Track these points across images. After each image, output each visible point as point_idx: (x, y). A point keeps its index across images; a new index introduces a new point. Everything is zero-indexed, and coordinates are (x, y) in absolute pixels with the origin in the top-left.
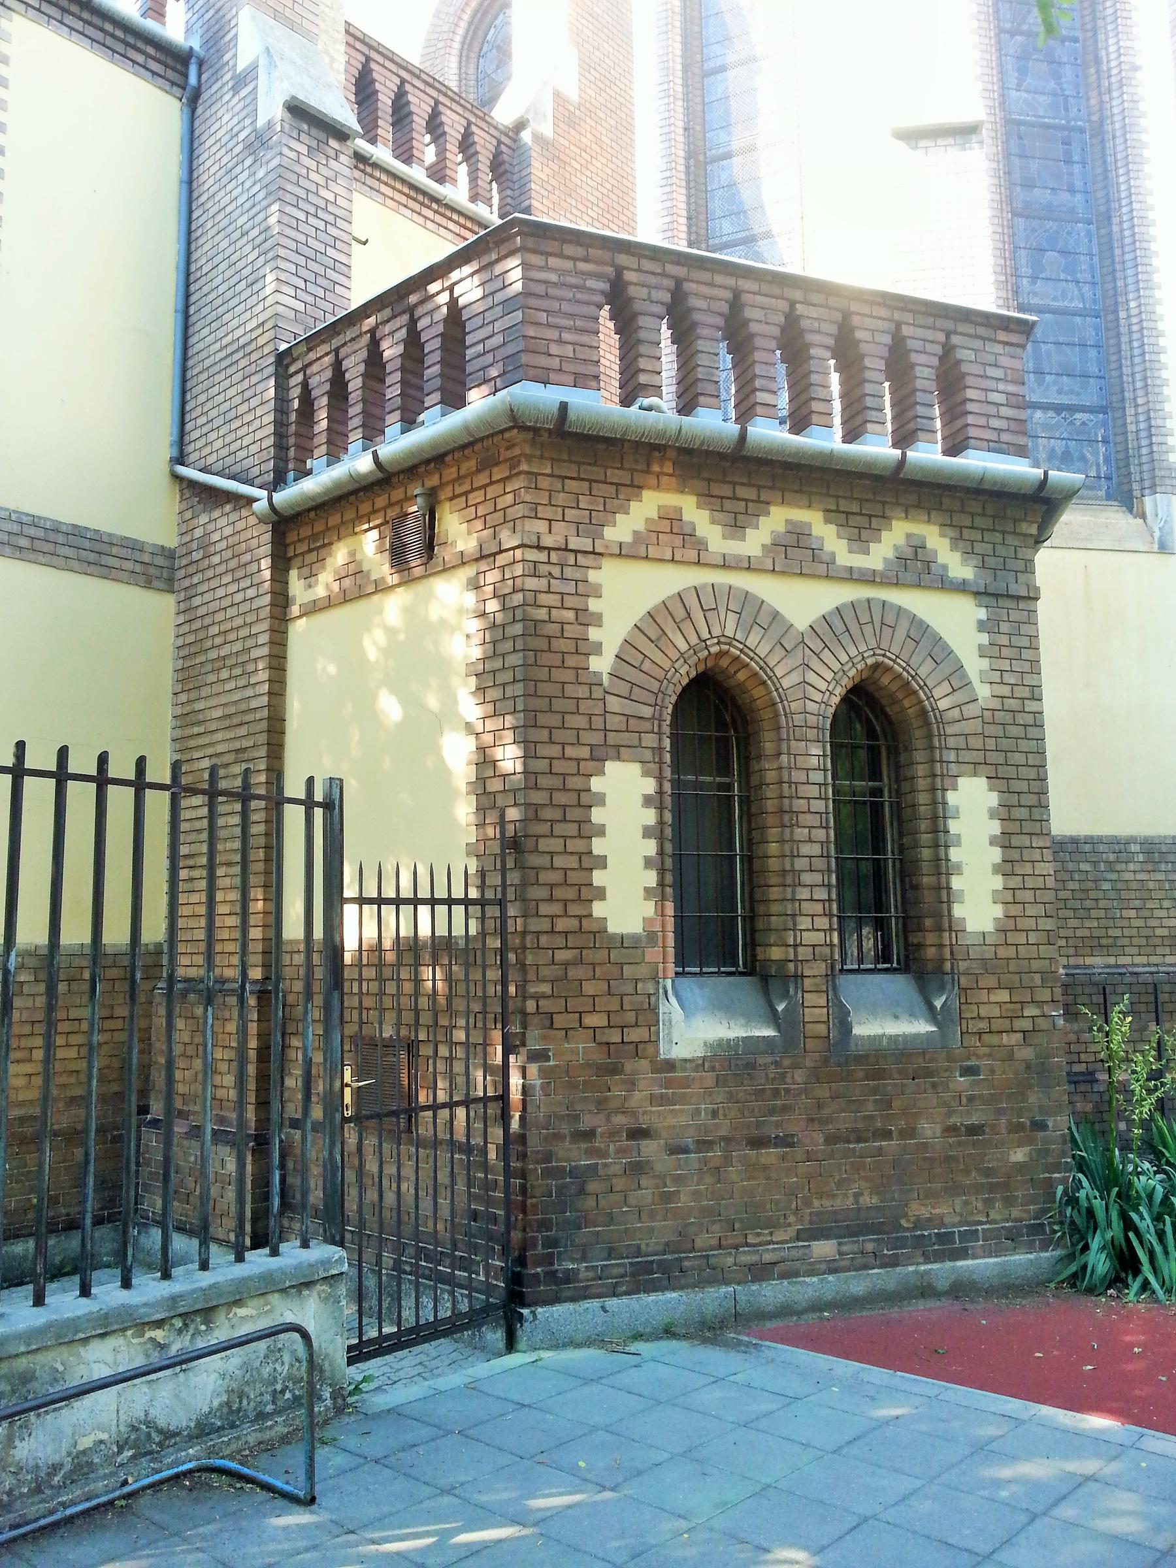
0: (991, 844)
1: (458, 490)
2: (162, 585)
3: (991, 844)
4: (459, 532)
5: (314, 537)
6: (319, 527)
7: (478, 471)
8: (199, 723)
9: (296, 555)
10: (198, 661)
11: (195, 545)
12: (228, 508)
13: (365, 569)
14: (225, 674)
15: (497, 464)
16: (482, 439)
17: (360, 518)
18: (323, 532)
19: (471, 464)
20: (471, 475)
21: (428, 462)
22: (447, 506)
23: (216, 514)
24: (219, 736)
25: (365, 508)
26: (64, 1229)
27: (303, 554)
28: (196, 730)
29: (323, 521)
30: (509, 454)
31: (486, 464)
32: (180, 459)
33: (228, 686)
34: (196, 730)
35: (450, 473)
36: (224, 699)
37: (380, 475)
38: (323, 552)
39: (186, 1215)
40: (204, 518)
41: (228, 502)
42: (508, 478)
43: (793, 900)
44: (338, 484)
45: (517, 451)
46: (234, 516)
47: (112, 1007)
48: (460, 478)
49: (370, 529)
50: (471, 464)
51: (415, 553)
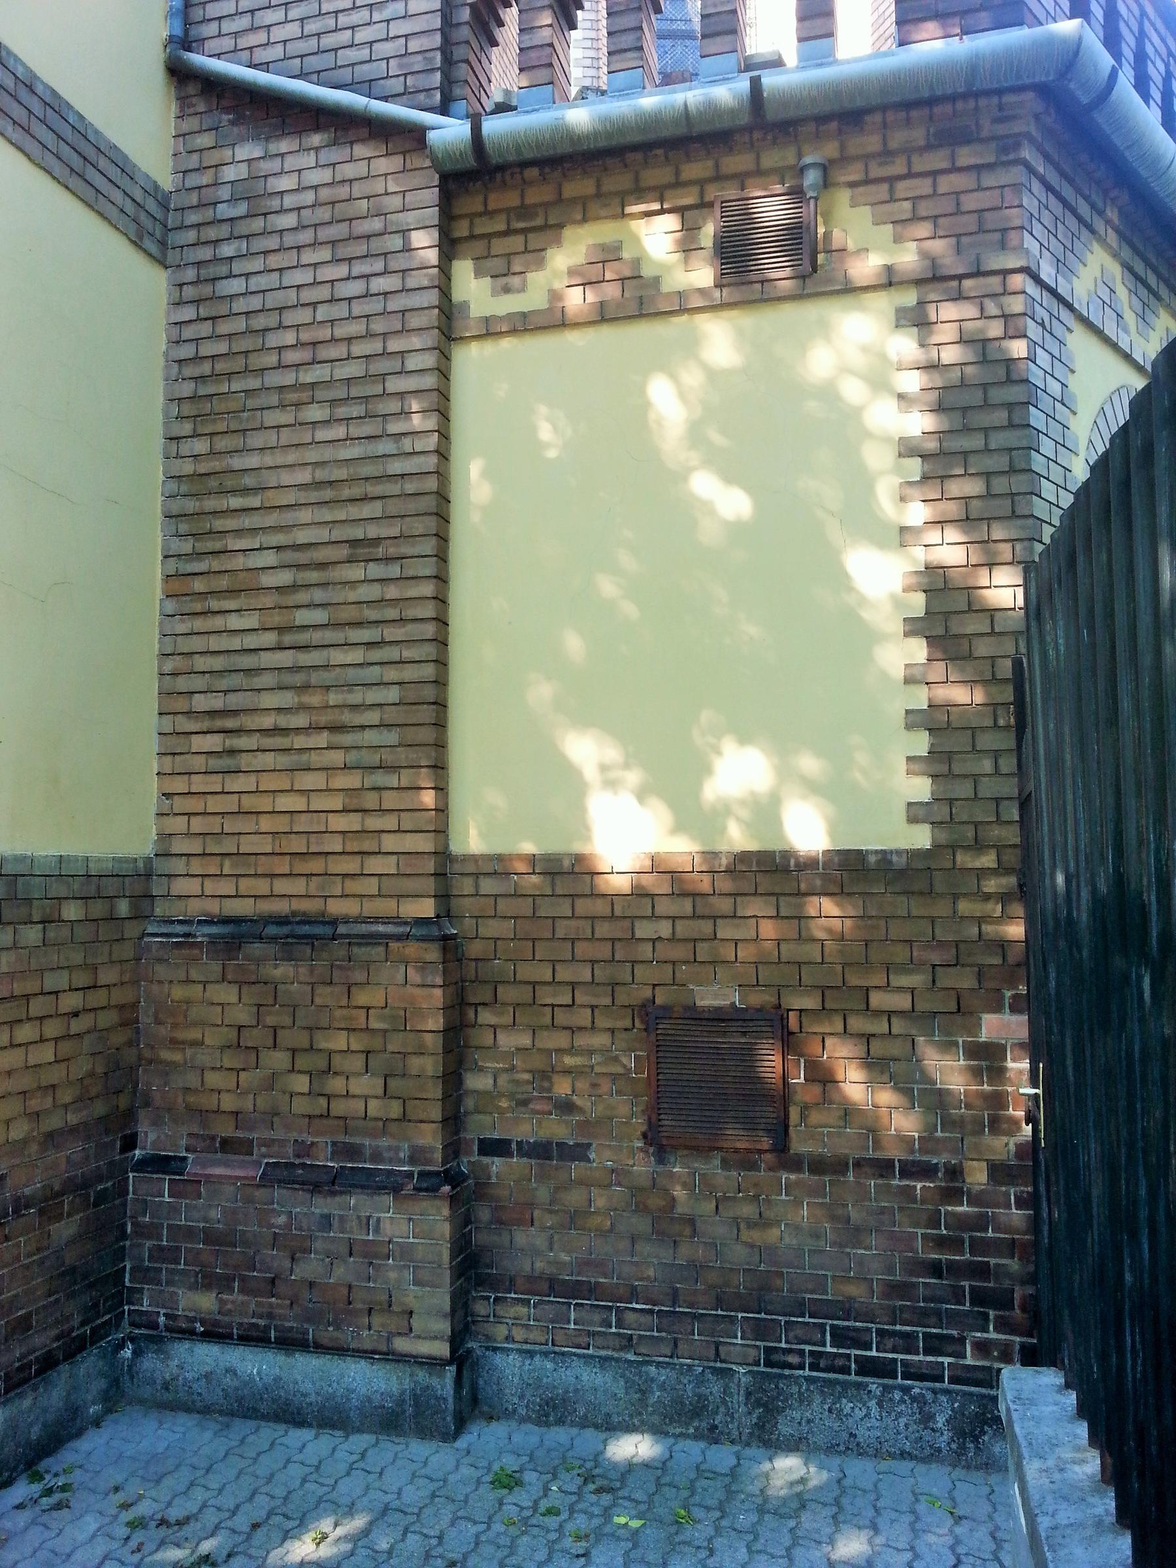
0: (909, 727)
1: (876, 171)
2: (153, 248)
3: (909, 727)
4: (869, 242)
5: (524, 211)
6: (534, 196)
7: (929, 147)
8: (246, 491)
9: (472, 237)
10: (235, 386)
11: (225, 193)
12: (316, 139)
13: (647, 272)
14: (315, 413)
15: (968, 142)
16: (953, 98)
17: (639, 193)
18: (546, 205)
19: (918, 135)
20: (908, 151)
21: (821, 119)
22: (843, 197)
23: (284, 146)
24: (305, 516)
25: (662, 175)
26: (39, 1373)
27: (488, 236)
28: (235, 502)
29: (480, 198)
30: (1001, 129)
31: (951, 137)
32: (185, 41)
33: (322, 434)
34: (235, 502)
35: (871, 142)
36: (312, 455)
37: (472, 162)
38: (535, 240)
39: (270, 1316)
40: (245, 151)
41: (317, 128)
42: (990, 167)
43: (951, 801)
44: (652, 121)
45: (1017, 127)
46: (334, 155)
47: (95, 968)
48: (887, 154)
49: (662, 212)
50: (918, 135)
51: (764, 266)
